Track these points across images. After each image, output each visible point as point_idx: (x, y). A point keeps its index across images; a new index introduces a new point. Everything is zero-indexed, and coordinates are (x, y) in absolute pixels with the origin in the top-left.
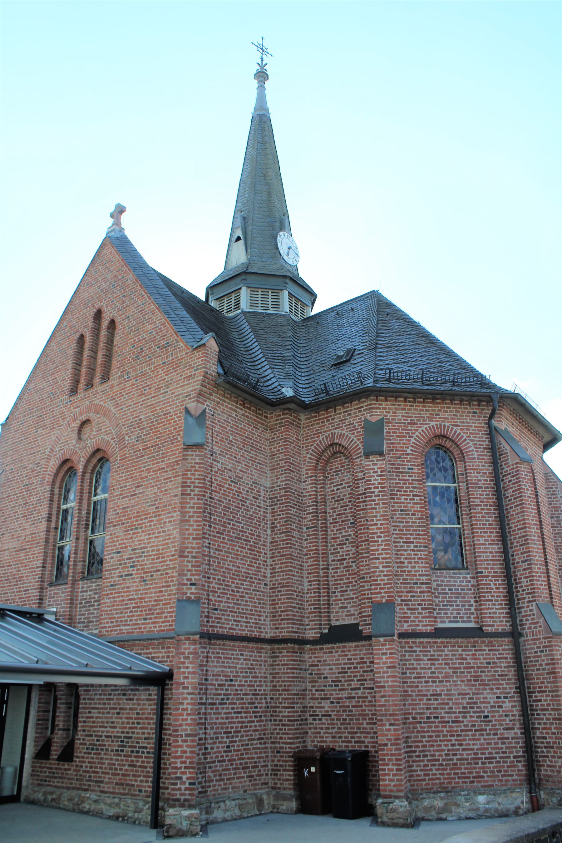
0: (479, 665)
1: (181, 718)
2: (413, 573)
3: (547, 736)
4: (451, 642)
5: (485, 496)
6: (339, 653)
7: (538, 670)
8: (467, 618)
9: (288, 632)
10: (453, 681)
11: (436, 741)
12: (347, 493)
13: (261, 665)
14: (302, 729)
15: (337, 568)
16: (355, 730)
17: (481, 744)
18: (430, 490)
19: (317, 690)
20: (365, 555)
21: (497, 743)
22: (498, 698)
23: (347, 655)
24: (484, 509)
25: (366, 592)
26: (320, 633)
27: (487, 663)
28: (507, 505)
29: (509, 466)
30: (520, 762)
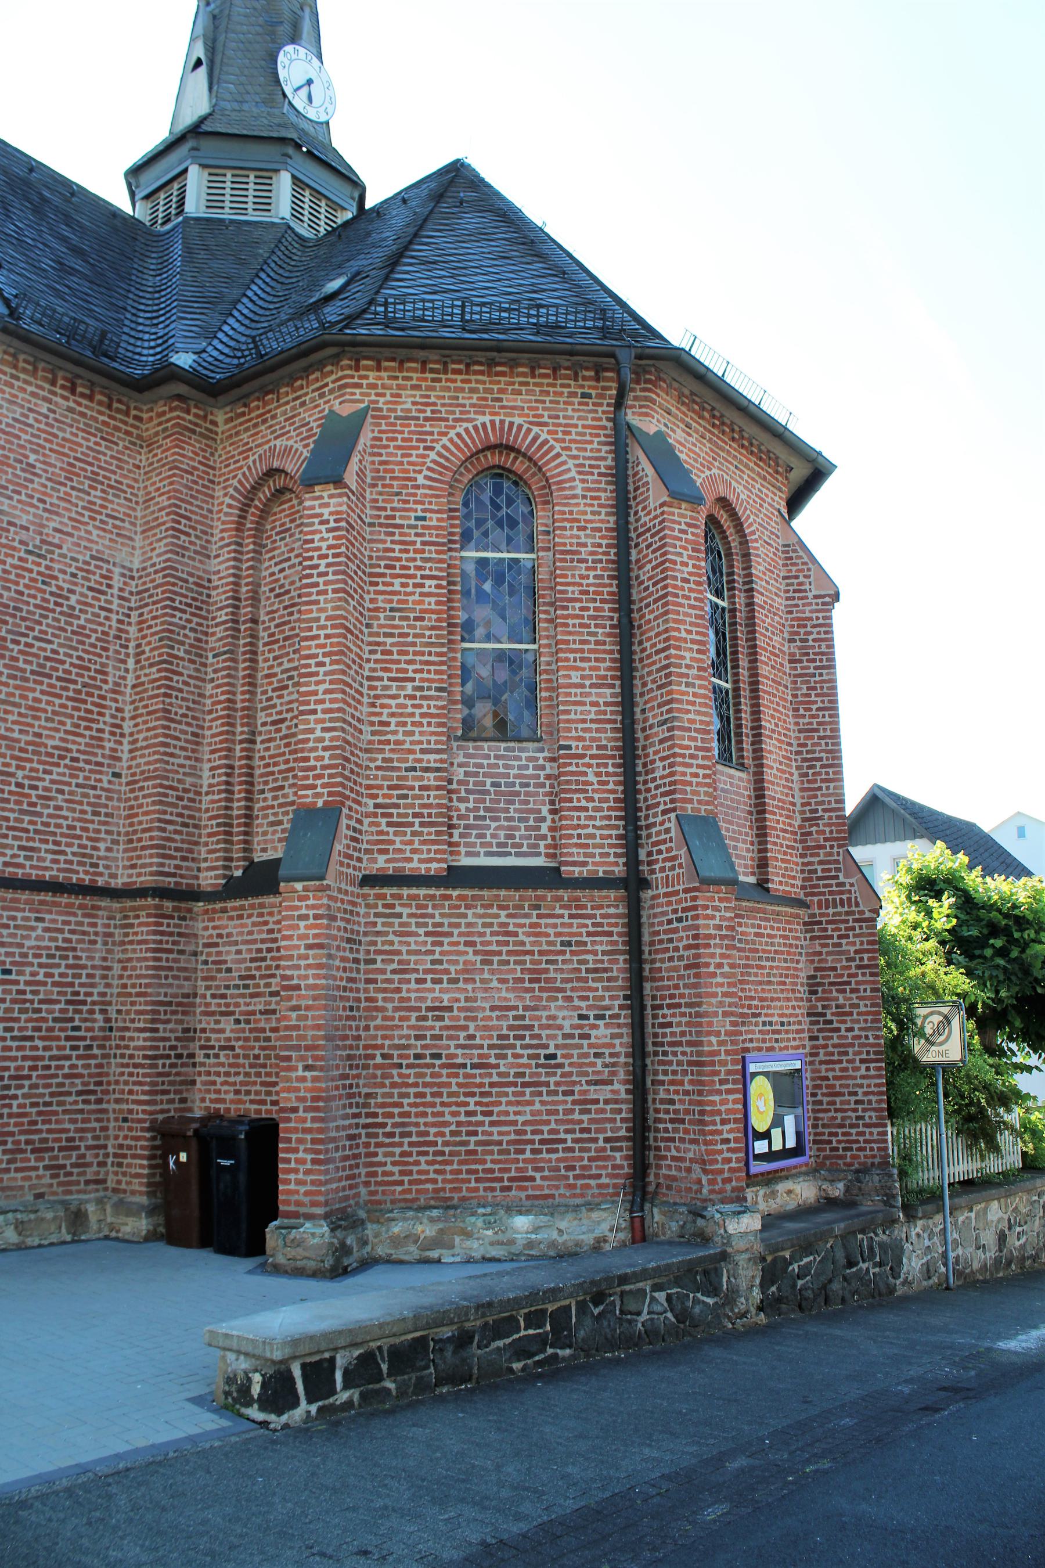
0: (545, 947)
2: (407, 746)
4: (482, 898)
5: (591, 581)
6: (254, 919)
7: (671, 959)
8: (529, 846)
9: (151, 874)
10: (482, 981)
11: (433, 1105)
13: (95, 942)
14: (178, 1074)
15: (270, 740)
17: (532, 1113)
18: (470, 568)
19: (213, 996)
21: (572, 1111)
22: (581, 1017)
24: (588, 609)
26: (224, 876)
27: (562, 944)
28: (641, 600)
30: (620, 1149)
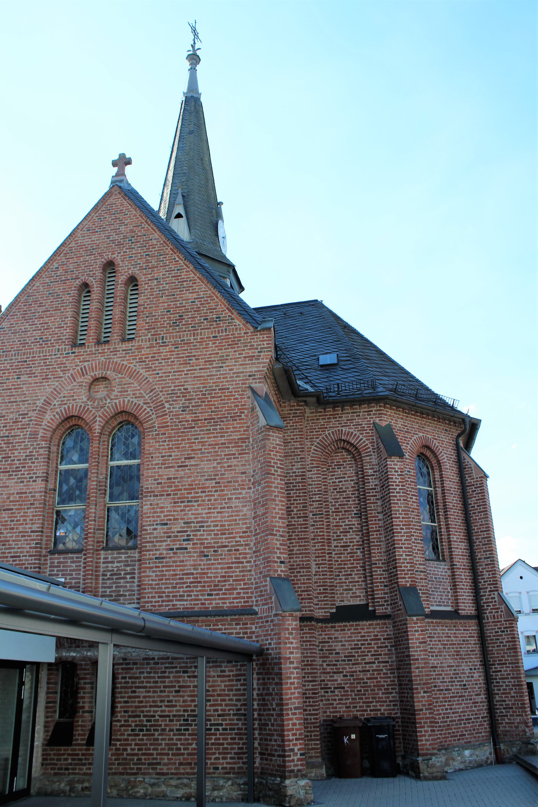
1: (289, 691)
3: (506, 699)
12: (350, 486)
15: (341, 554)
16: (371, 700)
19: (328, 665)
20: (376, 544)
23: (360, 633)
25: (379, 577)
29: (473, 479)
